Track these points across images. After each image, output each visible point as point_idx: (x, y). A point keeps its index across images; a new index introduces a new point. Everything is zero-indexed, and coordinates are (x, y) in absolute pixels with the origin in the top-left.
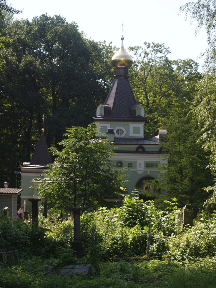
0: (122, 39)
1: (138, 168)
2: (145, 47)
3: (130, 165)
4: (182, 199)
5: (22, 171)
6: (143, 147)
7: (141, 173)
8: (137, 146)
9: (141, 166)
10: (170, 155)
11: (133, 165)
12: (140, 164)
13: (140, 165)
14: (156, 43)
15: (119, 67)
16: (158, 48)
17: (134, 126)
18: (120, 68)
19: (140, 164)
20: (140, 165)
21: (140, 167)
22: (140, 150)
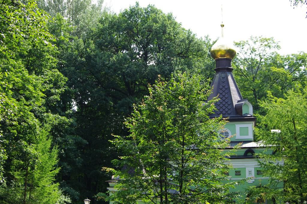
0: (222, 26)
1: (247, 176)
2: (251, 42)
3: (238, 173)
4: (21, 51)
5: (110, 186)
6: (252, 150)
7: (252, 182)
8: (245, 150)
9: (251, 174)
10: (288, 92)
11: (241, 173)
12: (250, 172)
13: (250, 173)
14: (264, 37)
15: (220, 58)
16: (267, 42)
17: (248, 136)
18: (220, 60)
19: (250, 172)
20: (250, 173)
21: (250, 175)
22: (249, 154)
